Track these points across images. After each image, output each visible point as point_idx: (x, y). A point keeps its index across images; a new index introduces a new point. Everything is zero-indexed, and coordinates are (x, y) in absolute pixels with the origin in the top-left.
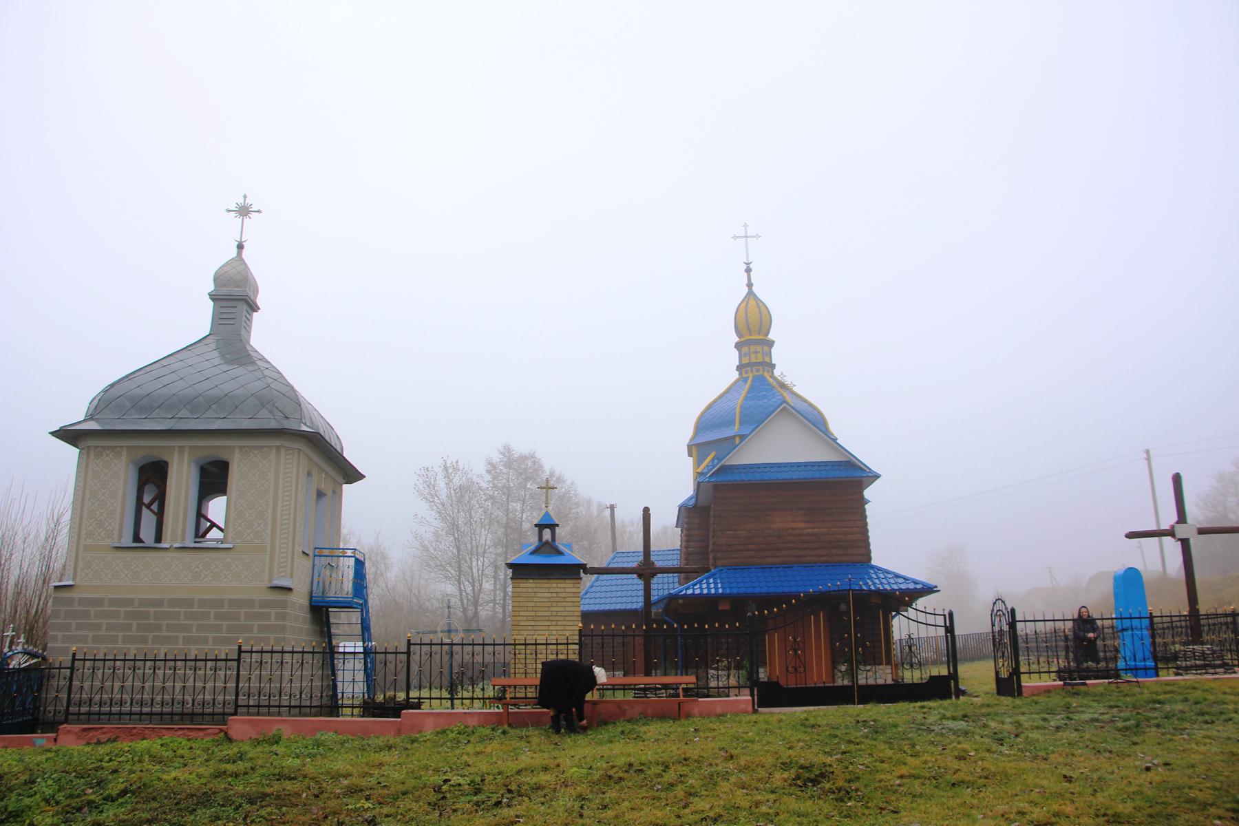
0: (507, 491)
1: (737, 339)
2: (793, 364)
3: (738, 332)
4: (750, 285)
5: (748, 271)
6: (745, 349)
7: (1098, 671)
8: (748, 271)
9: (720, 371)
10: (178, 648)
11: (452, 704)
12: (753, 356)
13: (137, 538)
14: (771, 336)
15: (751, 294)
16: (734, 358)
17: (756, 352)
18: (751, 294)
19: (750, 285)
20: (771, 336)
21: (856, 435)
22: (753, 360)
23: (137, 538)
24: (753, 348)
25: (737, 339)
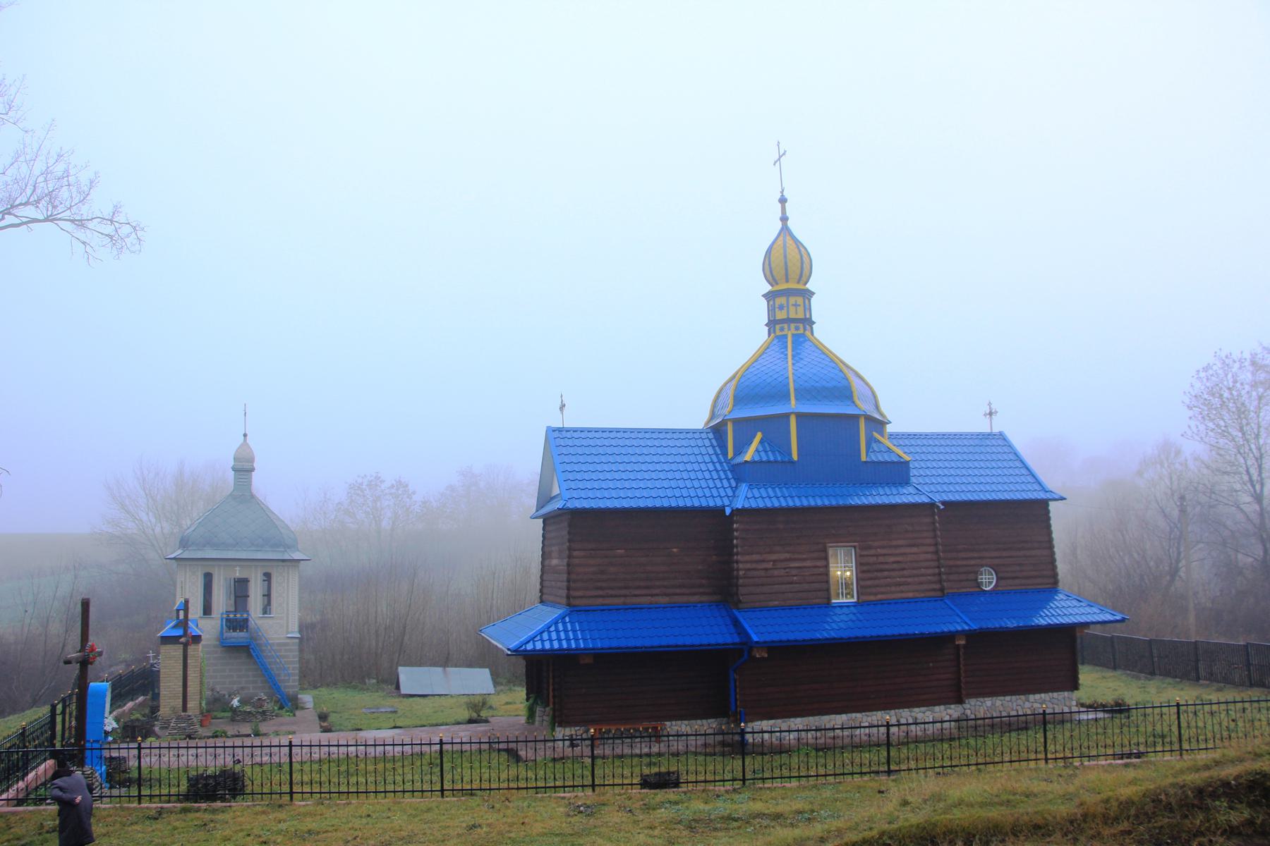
0: (138, 683)
1: (768, 288)
2: (838, 327)
3: (770, 276)
4: (784, 219)
5: (783, 201)
6: (781, 301)
7: (348, 766)
8: (783, 201)
9: (742, 335)
10: (538, 587)
11: (291, 799)
12: (792, 309)
13: (268, 577)
14: (809, 286)
15: (785, 230)
16: (760, 312)
17: (796, 305)
18: (785, 230)
19: (784, 219)
20: (809, 286)
21: (1053, 480)
22: (792, 316)
23: (268, 577)
24: (792, 300)
25: (768, 288)
